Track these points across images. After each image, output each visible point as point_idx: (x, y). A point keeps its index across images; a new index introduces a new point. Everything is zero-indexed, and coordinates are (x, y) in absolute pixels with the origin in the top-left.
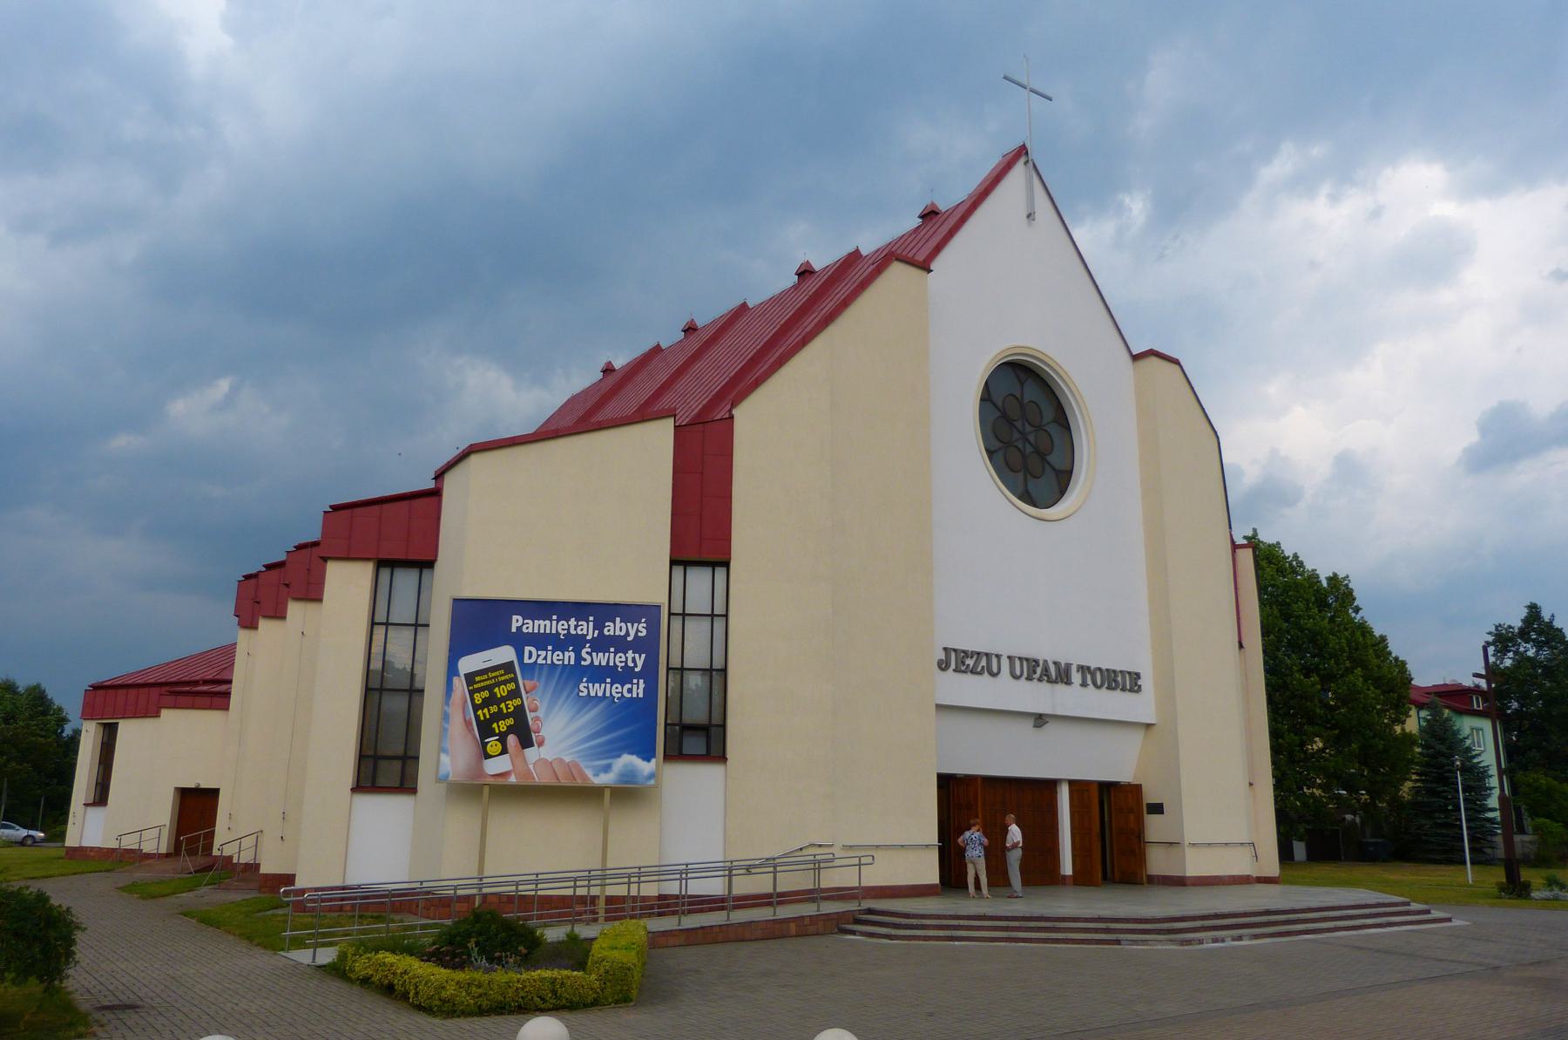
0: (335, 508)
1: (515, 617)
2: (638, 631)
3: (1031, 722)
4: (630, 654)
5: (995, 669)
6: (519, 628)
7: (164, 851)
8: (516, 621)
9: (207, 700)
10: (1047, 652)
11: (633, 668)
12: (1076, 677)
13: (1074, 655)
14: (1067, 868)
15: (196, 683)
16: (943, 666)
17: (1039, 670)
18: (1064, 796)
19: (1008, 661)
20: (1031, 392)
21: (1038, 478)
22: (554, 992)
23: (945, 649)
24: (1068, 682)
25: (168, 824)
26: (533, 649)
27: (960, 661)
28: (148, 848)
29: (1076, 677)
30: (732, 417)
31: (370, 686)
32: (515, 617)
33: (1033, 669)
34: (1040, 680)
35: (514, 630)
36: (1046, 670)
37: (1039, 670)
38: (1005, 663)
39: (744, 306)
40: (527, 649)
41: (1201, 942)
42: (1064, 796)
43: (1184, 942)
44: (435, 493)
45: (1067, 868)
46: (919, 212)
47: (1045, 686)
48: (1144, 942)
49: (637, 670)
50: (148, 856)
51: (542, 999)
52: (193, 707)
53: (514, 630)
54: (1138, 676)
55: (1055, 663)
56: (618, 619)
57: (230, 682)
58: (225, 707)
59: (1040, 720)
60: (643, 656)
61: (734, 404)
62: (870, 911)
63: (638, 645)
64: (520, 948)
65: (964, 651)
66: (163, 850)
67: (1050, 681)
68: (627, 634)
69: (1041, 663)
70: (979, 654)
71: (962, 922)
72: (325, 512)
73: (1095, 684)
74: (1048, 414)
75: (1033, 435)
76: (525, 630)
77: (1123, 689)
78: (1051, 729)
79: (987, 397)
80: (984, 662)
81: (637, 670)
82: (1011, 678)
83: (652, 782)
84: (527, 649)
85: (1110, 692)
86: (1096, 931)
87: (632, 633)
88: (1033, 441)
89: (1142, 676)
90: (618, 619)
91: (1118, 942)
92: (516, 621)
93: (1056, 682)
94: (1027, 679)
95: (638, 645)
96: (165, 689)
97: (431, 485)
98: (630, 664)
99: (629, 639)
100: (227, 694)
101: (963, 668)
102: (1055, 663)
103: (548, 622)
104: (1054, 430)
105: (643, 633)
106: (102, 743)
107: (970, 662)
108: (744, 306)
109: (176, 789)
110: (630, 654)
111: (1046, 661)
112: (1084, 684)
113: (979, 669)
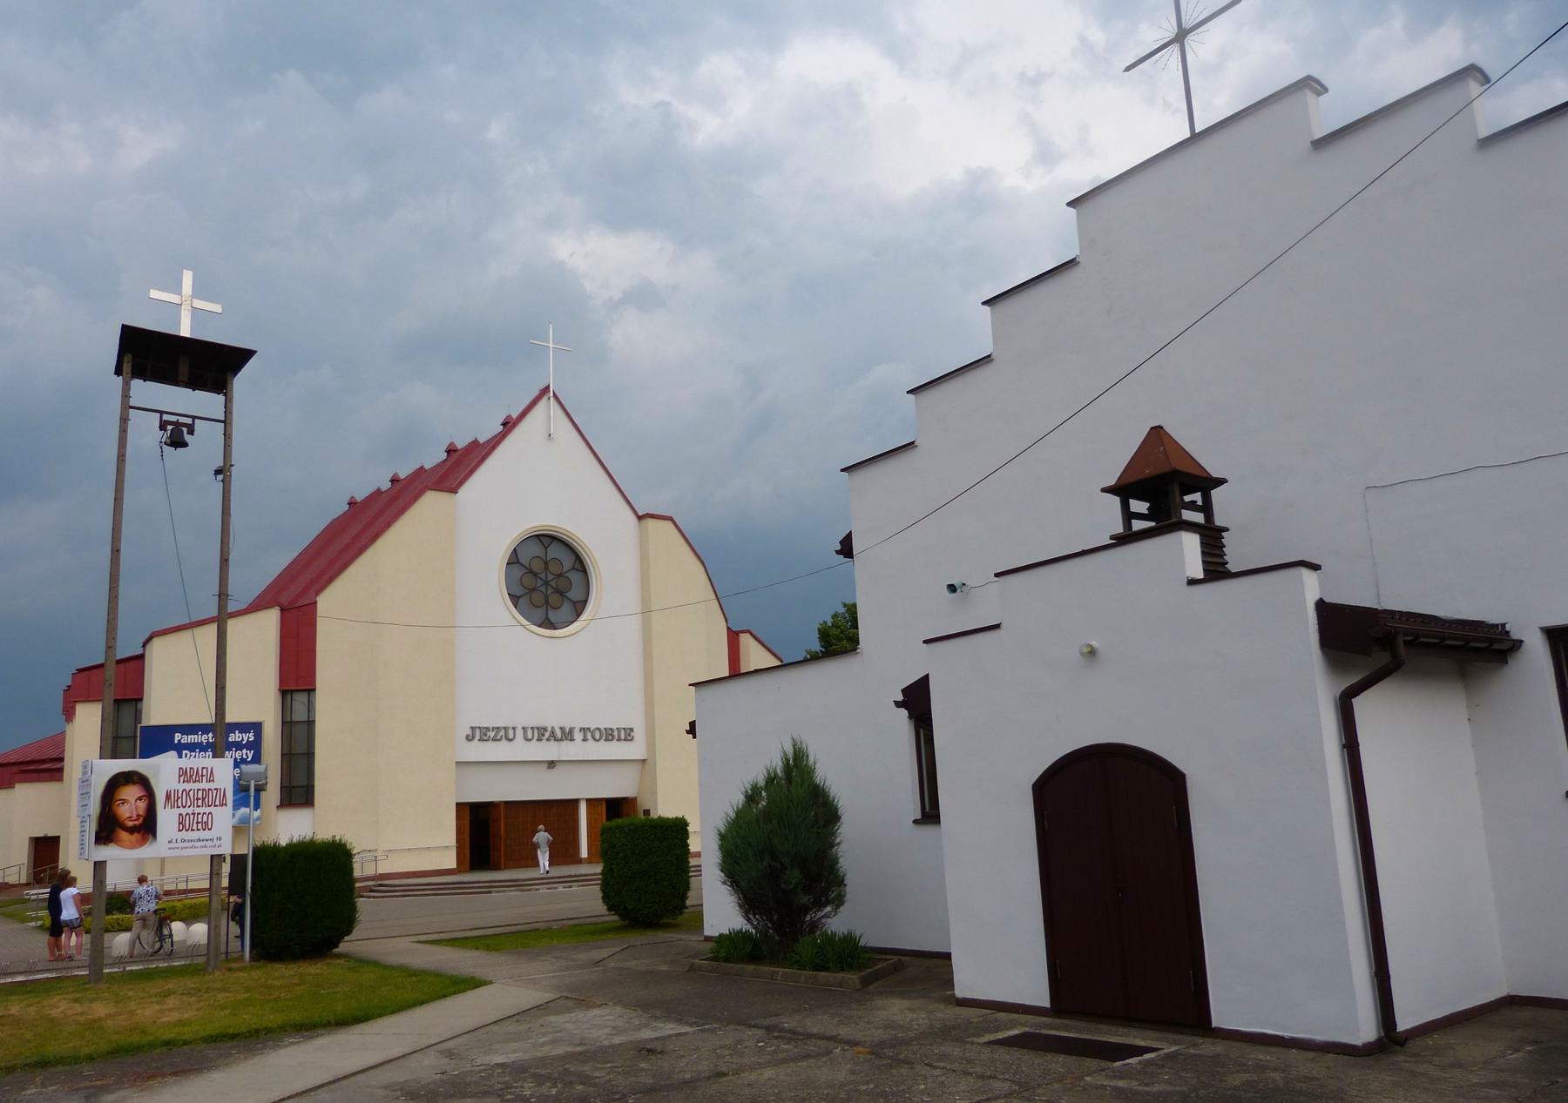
0: (80, 671)
1: (177, 735)
2: (249, 738)
3: (546, 766)
4: (244, 751)
5: (511, 736)
6: (179, 741)
7: (25, 882)
8: (178, 737)
9: (35, 775)
10: (553, 721)
11: (246, 759)
12: (578, 736)
13: (575, 721)
14: (584, 853)
15: (44, 761)
16: (469, 738)
17: (547, 735)
18: (583, 809)
19: (522, 731)
20: (555, 551)
21: (556, 609)
22: (118, 924)
23: (472, 728)
24: (572, 740)
25: (26, 862)
26: (188, 752)
27: (481, 734)
28: (12, 880)
29: (578, 736)
30: (316, 602)
31: (285, 720)
32: (177, 735)
33: (542, 733)
34: (548, 740)
35: (176, 742)
36: (553, 734)
37: (547, 735)
38: (520, 733)
39: (422, 468)
40: (184, 752)
41: (556, 888)
42: (583, 809)
43: (522, 891)
44: (141, 657)
45: (584, 853)
46: (501, 422)
47: (553, 743)
48: (503, 891)
49: (249, 760)
50: (13, 886)
51: (113, 927)
52: (38, 780)
53: (176, 742)
54: (632, 730)
55: (561, 728)
56: (237, 732)
57: (62, 759)
58: (60, 779)
59: (551, 764)
60: (252, 752)
61: (318, 593)
62: (381, 885)
63: (249, 746)
64: (953, 1034)
65: (485, 728)
66: (24, 880)
67: (556, 740)
68: (243, 740)
69: (549, 729)
70: (498, 728)
71: (397, 888)
72: (73, 674)
73: (594, 739)
74: (568, 562)
75: (555, 581)
76: (182, 742)
77: (619, 740)
78: (558, 769)
79: (514, 560)
80: (502, 733)
81: (249, 760)
82: (523, 740)
83: (258, 822)
84: (184, 752)
85: (607, 743)
86: (484, 887)
87: (246, 739)
88: (555, 586)
89: (635, 730)
90: (237, 732)
91: (490, 892)
92: (178, 737)
93: (561, 740)
94: (538, 740)
95: (249, 746)
96: (15, 769)
97: (140, 651)
98: (245, 757)
99: (244, 742)
100: (61, 770)
101: (486, 738)
102: (561, 728)
103: (196, 736)
104: (575, 577)
105: (252, 738)
106: (311, 691)
107: (492, 734)
108: (422, 468)
109: (30, 838)
110: (244, 751)
111: (553, 728)
112: (585, 740)
113: (499, 737)
